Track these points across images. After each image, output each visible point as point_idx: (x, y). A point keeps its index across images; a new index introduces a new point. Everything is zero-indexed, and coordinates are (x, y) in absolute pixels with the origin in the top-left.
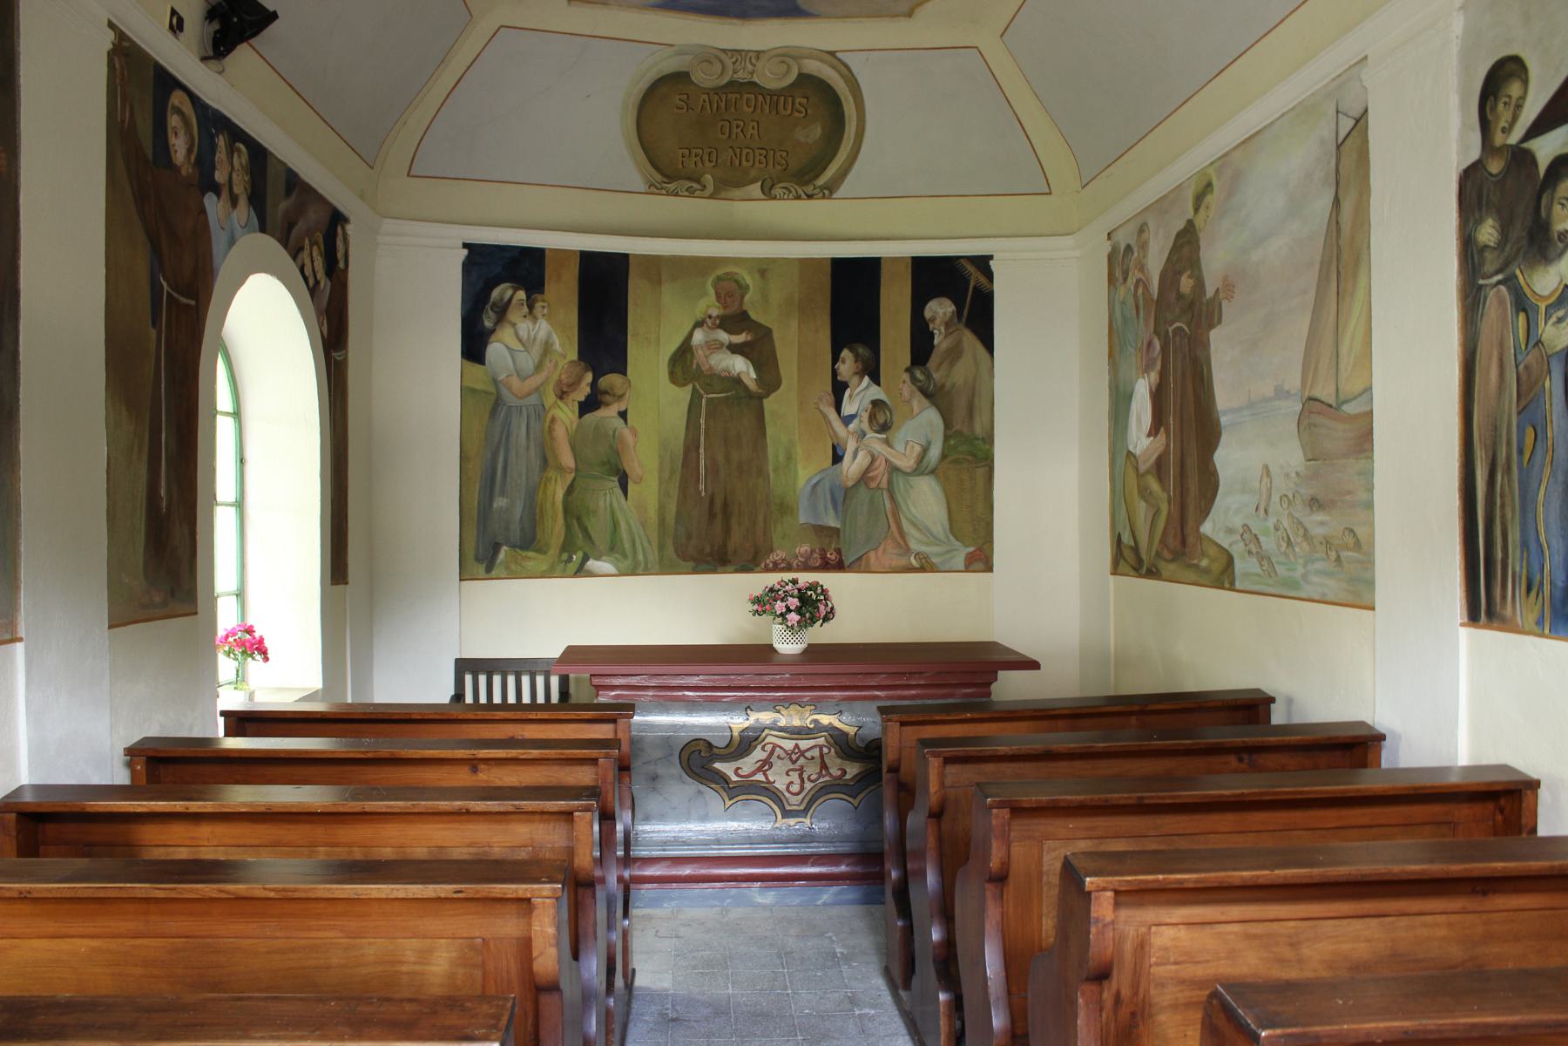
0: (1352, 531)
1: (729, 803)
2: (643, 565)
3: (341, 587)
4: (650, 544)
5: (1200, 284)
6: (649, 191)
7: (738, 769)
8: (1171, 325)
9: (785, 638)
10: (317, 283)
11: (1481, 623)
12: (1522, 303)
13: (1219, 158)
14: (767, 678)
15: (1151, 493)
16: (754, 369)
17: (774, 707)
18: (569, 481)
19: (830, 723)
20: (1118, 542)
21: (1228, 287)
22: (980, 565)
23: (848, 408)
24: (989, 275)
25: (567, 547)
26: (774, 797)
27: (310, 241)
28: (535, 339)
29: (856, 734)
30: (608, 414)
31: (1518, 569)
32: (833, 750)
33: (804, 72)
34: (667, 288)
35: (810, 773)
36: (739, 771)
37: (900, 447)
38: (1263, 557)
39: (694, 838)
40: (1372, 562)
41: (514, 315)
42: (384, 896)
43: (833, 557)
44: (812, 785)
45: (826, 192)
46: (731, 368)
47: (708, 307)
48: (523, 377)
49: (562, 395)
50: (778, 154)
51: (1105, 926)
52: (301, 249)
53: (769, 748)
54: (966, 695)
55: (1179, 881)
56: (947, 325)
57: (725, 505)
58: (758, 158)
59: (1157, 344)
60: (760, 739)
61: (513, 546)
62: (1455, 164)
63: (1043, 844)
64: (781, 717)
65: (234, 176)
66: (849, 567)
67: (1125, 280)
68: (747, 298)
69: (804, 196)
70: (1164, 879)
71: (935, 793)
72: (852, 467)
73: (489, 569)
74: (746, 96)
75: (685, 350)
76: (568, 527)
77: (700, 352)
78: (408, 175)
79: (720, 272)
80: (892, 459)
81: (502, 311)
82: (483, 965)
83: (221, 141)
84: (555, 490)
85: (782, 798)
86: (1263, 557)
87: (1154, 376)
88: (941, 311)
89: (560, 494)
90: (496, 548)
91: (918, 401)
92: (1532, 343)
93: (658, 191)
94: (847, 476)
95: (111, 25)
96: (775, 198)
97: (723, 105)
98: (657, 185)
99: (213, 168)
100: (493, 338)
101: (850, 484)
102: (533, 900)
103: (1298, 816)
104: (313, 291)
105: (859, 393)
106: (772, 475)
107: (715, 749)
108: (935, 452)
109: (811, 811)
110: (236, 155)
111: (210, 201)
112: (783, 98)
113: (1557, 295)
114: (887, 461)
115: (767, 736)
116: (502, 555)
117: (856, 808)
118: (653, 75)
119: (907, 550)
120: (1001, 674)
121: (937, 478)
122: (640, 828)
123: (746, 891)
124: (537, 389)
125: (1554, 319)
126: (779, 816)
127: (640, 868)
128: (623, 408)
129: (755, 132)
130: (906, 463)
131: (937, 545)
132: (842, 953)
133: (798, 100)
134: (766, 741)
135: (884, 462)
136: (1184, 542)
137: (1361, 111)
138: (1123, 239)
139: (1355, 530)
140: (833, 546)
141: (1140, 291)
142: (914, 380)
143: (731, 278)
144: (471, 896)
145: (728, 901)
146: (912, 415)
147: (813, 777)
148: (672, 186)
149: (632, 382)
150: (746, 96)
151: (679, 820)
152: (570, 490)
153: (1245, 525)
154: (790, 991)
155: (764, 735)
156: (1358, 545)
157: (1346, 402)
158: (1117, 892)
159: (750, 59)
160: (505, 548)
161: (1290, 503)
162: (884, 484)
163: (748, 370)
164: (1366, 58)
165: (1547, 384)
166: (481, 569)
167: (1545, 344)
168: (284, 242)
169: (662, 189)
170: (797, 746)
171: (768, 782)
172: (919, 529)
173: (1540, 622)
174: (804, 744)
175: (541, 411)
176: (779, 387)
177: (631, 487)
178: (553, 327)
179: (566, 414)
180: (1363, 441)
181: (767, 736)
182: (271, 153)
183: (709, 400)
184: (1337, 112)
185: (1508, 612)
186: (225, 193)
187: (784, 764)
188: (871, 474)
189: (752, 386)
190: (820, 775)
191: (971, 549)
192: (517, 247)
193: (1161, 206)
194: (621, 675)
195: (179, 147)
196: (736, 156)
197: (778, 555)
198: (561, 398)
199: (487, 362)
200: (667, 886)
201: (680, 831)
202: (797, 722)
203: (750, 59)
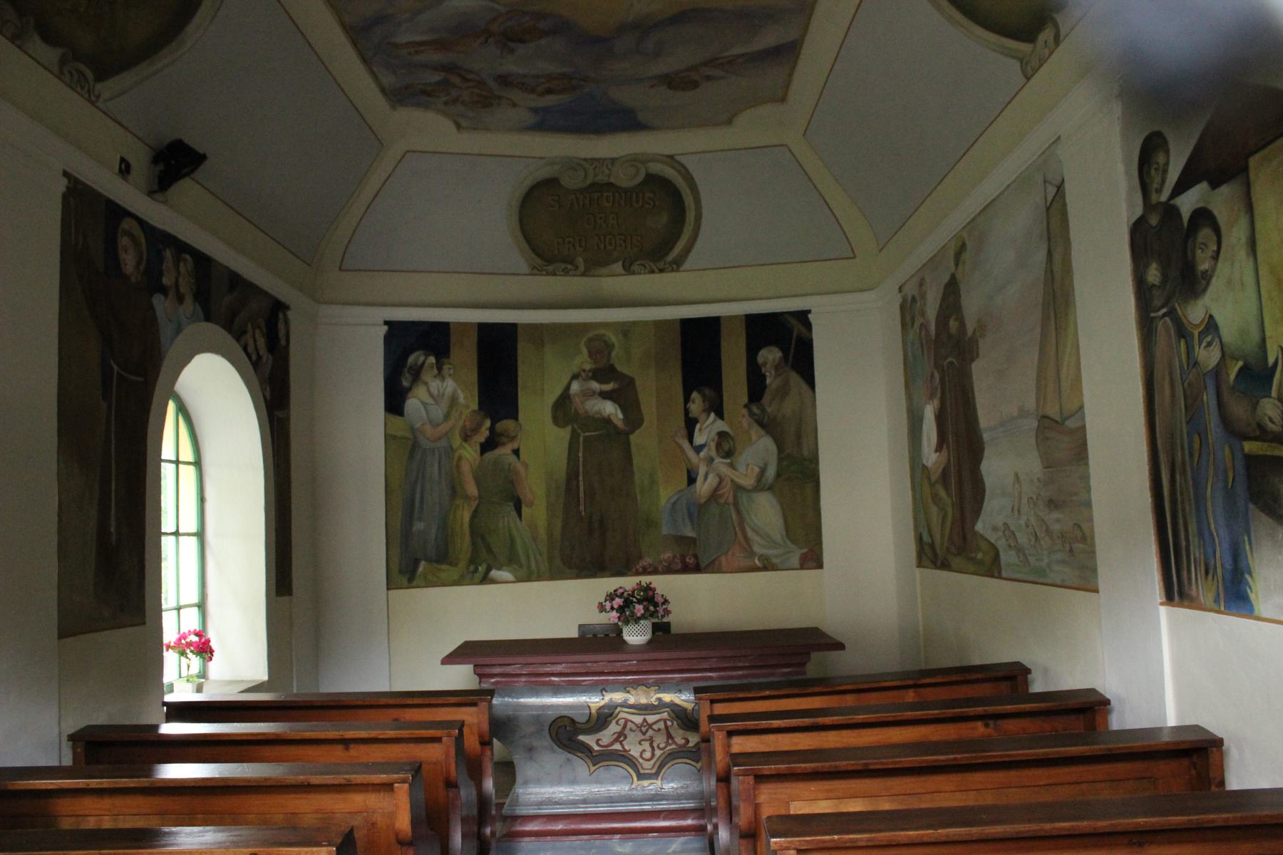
0: (1079, 526)
1: (593, 768)
3: (286, 598)
4: (541, 555)
5: (962, 325)
7: (598, 740)
8: (945, 360)
9: (639, 632)
10: (259, 357)
11: (1175, 603)
12: (1182, 331)
13: (969, 223)
14: (619, 664)
15: (940, 499)
16: (622, 411)
17: (625, 689)
18: (474, 508)
19: (672, 701)
20: (920, 540)
21: (982, 327)
23: (699, 439)
24: (808, 326)
25: (474, 560)
26: (630, 763)
28: (443, 395)
29: (693, 709)
30: (504, 451)
31: (1197, 555)
32: (675, 723)
33: (651, 171)
36: (600, 742)
37: (742, 469)
38: (1019, 550)
40: (1094, 552)
41: (427, 376)
43: (691, 561)
44: (661, 752)
45: (675, 266)
46: (603, 411)
48: (435, 425)
49: (466, 438)
52: (244, 332)
53: (622, 722)
54: (785, 674)
55: (852, 841)
56: (777, 368)
59: (937, 376)
60: (614, 715)
61: (429, 560)
62: (1126, 220)
63: (789, 804)
64: (630, 696)
65: (181, 280)
66: (705, 568)
67: (913, 324)
68: (614, 354)
69: (656, 270)
70: (839, 839)
71: (721, 760)
72: (704, 487)
73: (410, 580)
74: (605, 194)
75: (564, 399)
76: (474, 544)
77: (577, 400)
78: (340, 269)
79: (590, 335)
80: (736, 479)
81: (417, 373)
83: (168, 254)
84: (462, 515)
85: (637, 763)
86: (1019, 550)
87: (936, 402)
88: (771, 357)
89: (466, 517)
90: (416, 562)
91: (756, 431)
92: (1191, 365)
93: (538, 272)
94: (700, 495)
95: (66, 174)
96: (634, 273)
97: (587, 202)
98: (539, 268)
99: (161, 274)
100: (410, 394)
101: (703, 501)
103: (1013, 775)
104: (256, 364)
105: (708, 426)
106: (639, 497)
108: (771, 472)
109: (662, 774)
110: (182, 264)
111: (158, 302)
112: (635, 195)
113: (1205, 323)
114: (732, 481)
115: (619, 712)
116: (421, 569)
117: (699, 771)
118: (529, 183)
119: (752, 554)
122: (521, 791)
123: (609, 842)
124: (446, 434)
125: (1204, 344)
126: (635, 778)
127: (521, 824)
130: (748, 482)
134: (619, 717)
136: (964, 538)
137: (1060, 179)
138: (911, 290)
139: (1082, 525)
140: (691, 552)
142: (751, 414)
143: (599, 338)
147: (662, 746)
148: (550, 268)
150: (605, 194)
151: (552, 784)
152: (475, 515)
153: (1005, 524)
156: (1084, 539)
157: (1068, 418)
159: (607, 166)
160: (423, 563)
161: (1035, 504)
162: (731, 500)
164: (1059, 138)
165: (1205, 397)
166: (405, 581)
167: (1201, 365)
170: (645, 720)
171: (625, 751)
172: (761, 536)
173: (1217, 600)
174: (651, 719)
176: (642, 424)
177: (525, 510)
179: (470, 453)
180: (1081, 453)
181: (619, 712)
182: (215, 261)
183: (586, 439)
184: (1045, 182)
185: (1194, 593)
186: (172, 294)
187: (636, 735)
188: (719, 493)
189: (620, 424)
190: (667, 744)
191: (805, 550)
192: (428, 322)
193: (933, 262)
195: (129, 261)
196: (601, 241)
197: (646, 561)
200: (542, 839)
201: (553, 793)
202: (643, 701)
203: (607, 166)
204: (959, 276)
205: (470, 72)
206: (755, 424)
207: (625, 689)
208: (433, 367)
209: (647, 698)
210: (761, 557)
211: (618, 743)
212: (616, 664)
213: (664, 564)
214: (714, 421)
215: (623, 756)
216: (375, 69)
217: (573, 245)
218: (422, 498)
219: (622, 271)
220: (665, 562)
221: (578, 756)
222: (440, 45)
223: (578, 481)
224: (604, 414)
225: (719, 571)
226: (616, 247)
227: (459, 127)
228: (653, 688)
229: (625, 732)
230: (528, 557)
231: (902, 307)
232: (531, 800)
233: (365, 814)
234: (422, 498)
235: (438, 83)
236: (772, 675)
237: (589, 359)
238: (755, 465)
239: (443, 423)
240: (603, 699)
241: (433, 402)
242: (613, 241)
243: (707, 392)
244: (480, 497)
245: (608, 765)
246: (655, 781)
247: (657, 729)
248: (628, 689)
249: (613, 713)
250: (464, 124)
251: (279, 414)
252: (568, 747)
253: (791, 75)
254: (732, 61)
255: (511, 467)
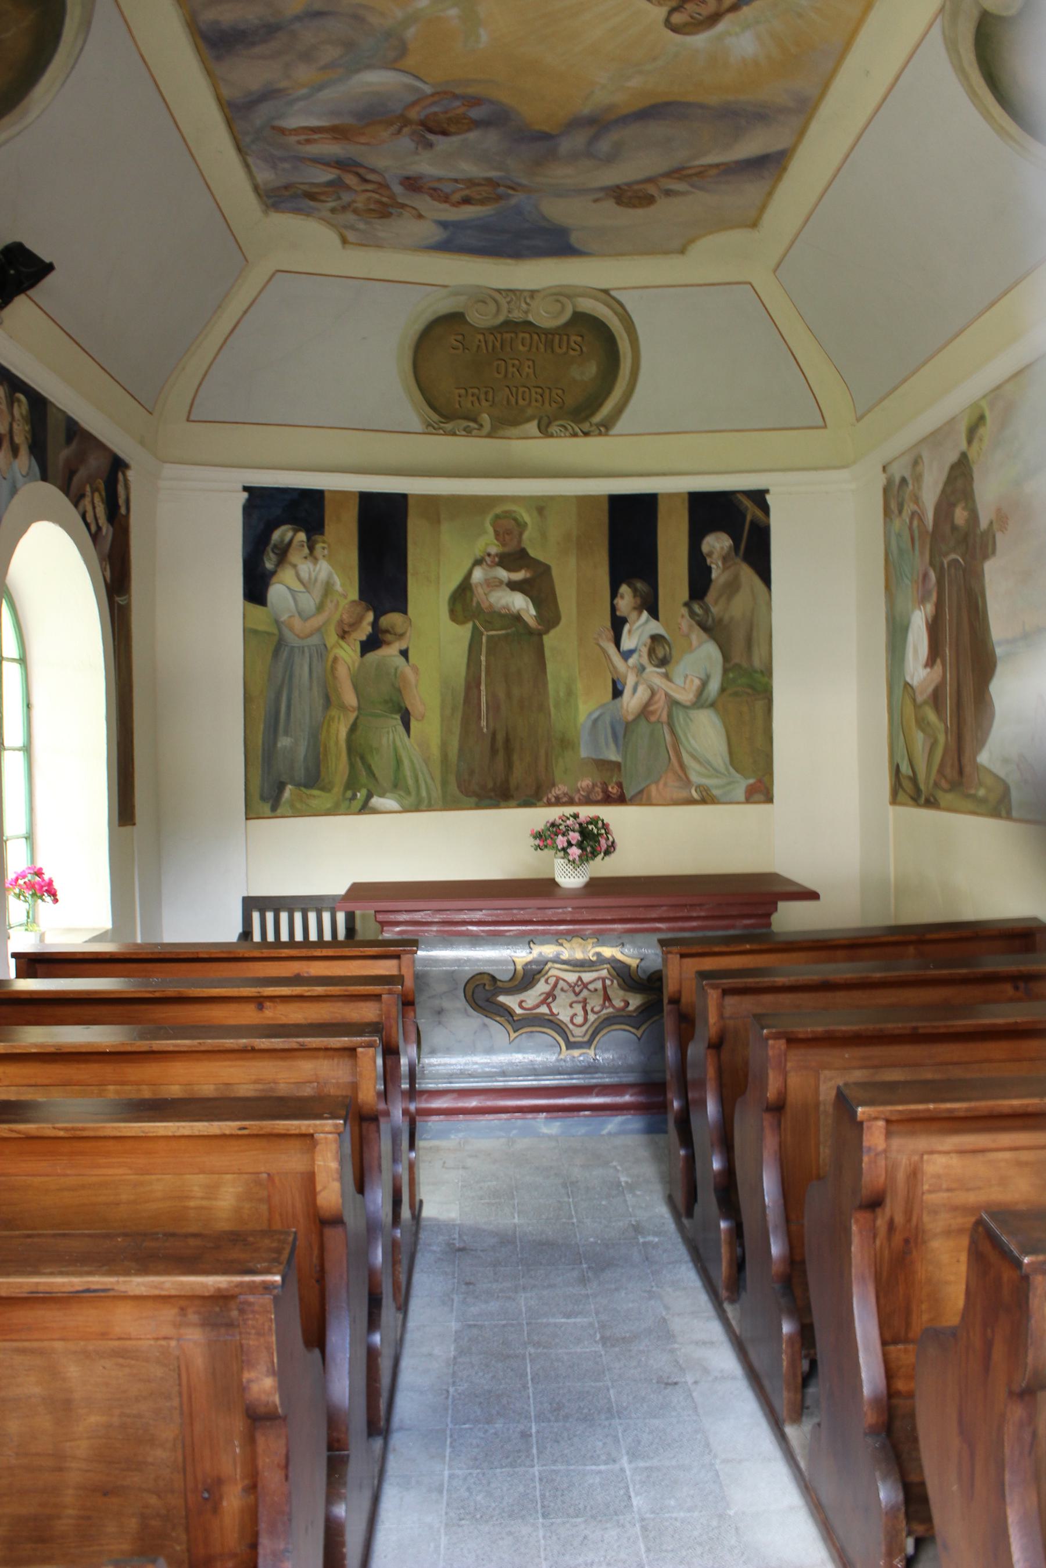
1: (513, 1035)
2: (426, 802)
3: (129, 828)
6: (426, 431)
7: (522, 1002)
14: (550, 912)
15: (928, 723)
17: (557, 941)
20: (896, 772)
21: (1002, 519)
22: (762, 797)
23: (628, 642)
24: (765, 508)
25: (352, 784)
27: (91, 488)
28: (316, 580)
29: (638, 966)
30: (389, 653)
32: (615, 982)
33: (580, 309)
34: (445, 527)
35: (593, 1005)
36: (524, 1004)
37: (679, 680)
39: (480, 1070)
41: (296, 556)
42: (170, 1134)
43: (615, 791)
44: (596, 1016)
45: (603, 429)
46: (511, 605)
47: (487, 545)
48: (304, 617)
49: (343, 635)
50: (554, 392)
51: (877, 1155)
52: (82, 496)
53: (552, 981)
54: (746, 927)
56: (725, 559)
57: (507, 741)
58: (534, 395)
59: (933, 576)
60: (543, 972)
61: (298, 785)
64: (563, 949)
65: (15, 426)
66: (631, 800)
67: (900, 512)
68: (526, 535)
69: (580, 433)
70: (935, 1108)
71: (715, 1024)
72: (632, 701)
73: (274, 808)
74: (521, 335)
75: (465, 589)
76: (352, 766)
77: (480, 591)
79: (498, 510)
81: (283, 552)
82: (269, 1200)
85: (566, 1030)
87: (930, 608)
88: (718, 546)
89: (343, 731)
90: (281, 787)
91: (697, 635)
93: (434, 431)
94: (628, 711)
96: (552, 436)
97: (498, 345)
100: (274, 579)
101: (630, 718)
102: (316, 1136)
104: (95, 537)
106: (553, 710)
107: (499, 984)
108: (714, 686)
109: (595, 1042)
110: (16, 405)
114: (667, 695)
115: (550, 969)
117: (639, 1039)
118: (428, 316)
119: (688, 783)
120: (782, 905)
121: (717, 711)
123: (532, 1122)
124: (319, 630)
127: (427, 1101)
128: (404, 647)
129: (531, 371)
130: (686, 697)
131: (717, 777)
132: (626, 1183)
133: (573, 338)
134: (550, 974)
135: (663, 696)
136: (961, 772)
138: (898, 471)
140: (614, 780)
141: (915, 523)
142: (692, 614)
143: (508, 515)
144: (255, 1132)
145: (514, 1132)
146: (690, 649)
147: (597, 1009)
148: (449, 426)
149: (412, 620)
151: (464, 1052)
152: (353, 729)
154: (575, 1220)
155: (547, 967)
158: (888, 1121)
160: (289, 787)
162: (664, 717)
163: (528, 607)
166: (266, 808)
168: (66, 489)
169: (440, 428)
171: (553, 1014)
174: (587, 977)
175: (323, 650)
177: (413, 724)
178: (333, 566)
179: (348, 653)
181: (550, 969)
183: (489, 638)
188: (651, 708)
190: (603, 1007)
191: (751, 781)
193: (935, 438)
194: (406, 911)
197: (560, 789)
198: (343, 637)
199: (269, 603)
201: (466, 1064)
202: (579, 955)
204: (972, 455)
205: (373, 171)
206: (697, 628)
207: (557, 941)
208: (303, 546)
209: (583, 953)
210: (698, 788)
211: (545, 1006)
212: (547, 911)
213: (582, 793)
214: (647, 621)
215: (549, 1020)
216: (250, 160)
217: (478, 399)
218: (289, 707)
219: (538, 434)
220: (583, 791)
221: (496, 1021)
222: (338, 133)
223: (480, 691)
224: (513, 609)
225: (649, 803)
226: (530, 401)
227: (344, 241)
228: (590, 941)
229: (555, 993)
230: (417, 781)
231: (886, 491)
232: (440, 1072)
233: (316, 1084)
234: (289, 707)
235: (330, 184)
236: (733, 927)
237: (495, 542)
238: (697, 677)
239: (314, 615)
240: (531, 953)
241: (302, 589)
242: (527, 396)
243: (639, 585)
244: (359, 708)
245: (532, 1032)
246: (588, 1051)
247: (593, 989)
248: (560, 941)
249: (543, 969)
250: (351, 236)
251: (120, 600)
252: (484, 1010)
253: (770, 194)
254: (702, 172)
255: (399, 672)
